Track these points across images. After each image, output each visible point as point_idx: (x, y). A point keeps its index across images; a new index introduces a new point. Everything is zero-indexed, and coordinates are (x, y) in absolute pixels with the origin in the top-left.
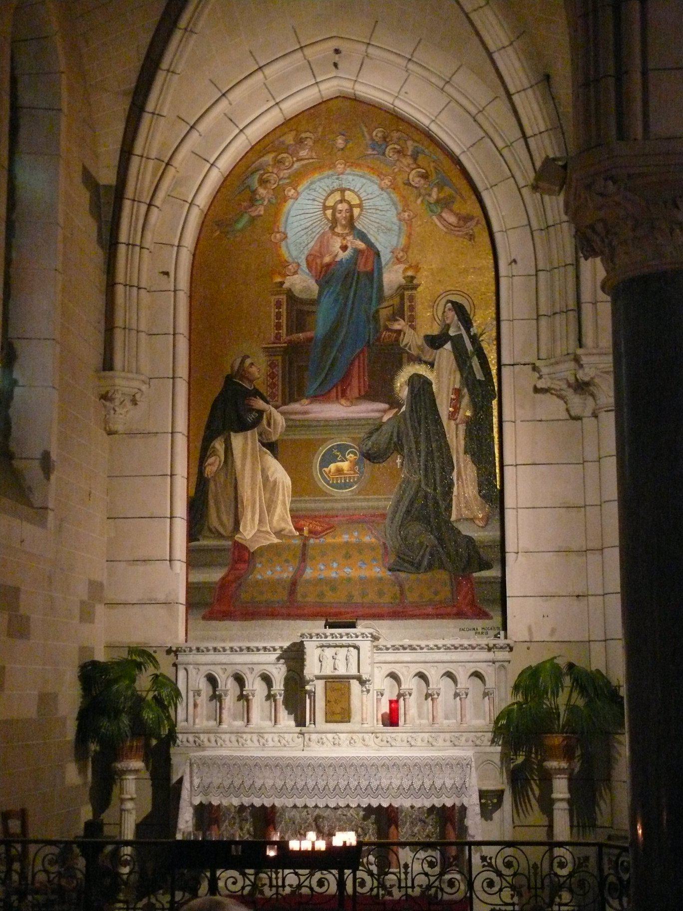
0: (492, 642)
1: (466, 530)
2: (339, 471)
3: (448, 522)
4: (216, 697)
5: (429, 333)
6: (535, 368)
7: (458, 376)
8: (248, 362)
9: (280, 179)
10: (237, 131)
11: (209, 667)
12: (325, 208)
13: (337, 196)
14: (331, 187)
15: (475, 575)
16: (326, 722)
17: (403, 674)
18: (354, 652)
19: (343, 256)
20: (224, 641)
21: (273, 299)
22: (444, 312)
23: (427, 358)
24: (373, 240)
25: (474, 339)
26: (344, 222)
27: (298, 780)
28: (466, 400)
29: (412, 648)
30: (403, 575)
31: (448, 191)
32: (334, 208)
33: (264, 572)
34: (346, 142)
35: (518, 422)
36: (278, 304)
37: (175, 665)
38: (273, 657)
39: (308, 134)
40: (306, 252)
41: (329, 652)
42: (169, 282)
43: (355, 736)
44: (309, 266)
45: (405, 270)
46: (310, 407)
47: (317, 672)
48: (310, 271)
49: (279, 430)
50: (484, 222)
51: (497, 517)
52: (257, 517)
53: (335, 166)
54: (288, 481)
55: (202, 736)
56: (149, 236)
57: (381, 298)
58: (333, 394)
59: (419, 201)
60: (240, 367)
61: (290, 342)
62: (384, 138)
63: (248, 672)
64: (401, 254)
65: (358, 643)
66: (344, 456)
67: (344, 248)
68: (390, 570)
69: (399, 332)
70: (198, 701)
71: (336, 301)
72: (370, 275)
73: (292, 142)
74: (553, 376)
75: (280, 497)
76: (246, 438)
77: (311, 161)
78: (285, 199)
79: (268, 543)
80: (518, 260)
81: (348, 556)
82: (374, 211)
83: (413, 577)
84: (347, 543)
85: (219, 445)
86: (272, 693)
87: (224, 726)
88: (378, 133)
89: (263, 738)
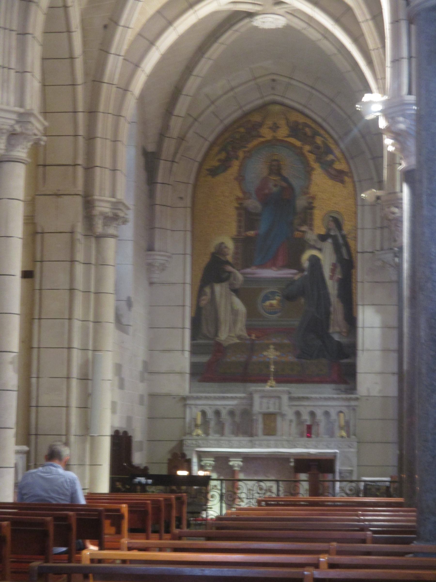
2: (271, 305)
11: (203, 407)
19: (275, 189)
41: (265, 400)
85: (207, 290)
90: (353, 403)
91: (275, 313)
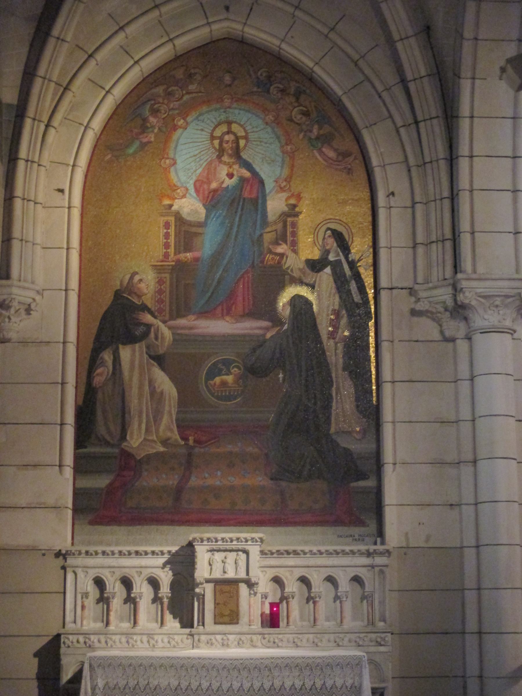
0: (372, 548)
1: (344, 442)
2: (224, 384)
3: (328, 435)
4: (103, 599)
5: (310, 257)
6: (412, 291)
7: (337, 299)
8: (137, 278)
9: (170, 110)
10: (132, 62)
11: (97, 570)
12: (213, 138)
13: (224, 128)
14: (218, 119)
15: (354, 484)
16: (215, 623)
17: (286, 578)
18: (243, 556)
19: (229, 182)
20: (109, 545)
21: (162, 220)
22: (324, 239)
23: (309, 280)
24: (258, 169)
25: (352, 265)
26: (230, 152)
27: (193, 681)
28: (344, 321)
29: (295, 553)
30: (284, 484)
31: (327, 129)
32: (221, 139)
33: (150, 480)
34: (234, 79)
35: (396, 341)
36: (167, 225)
37: (64, 568)
38: (161, 561)
39: (197, 70)
40: (194, 178)
41: (218, 557)
42: (64, 199)
43: (243, 637)
44: (197, 191)
45: (287, 199)
46: (195, 322)
47: (207, 575)
48: (198, 195)
49: (166, 344)
50: (360, 157)
51: (373, 430)
52: (144, 426)
53: (222, 101)
54: (174, 392)
55: (92, 637)
56: (46, 154)
57: (265, 222)
58: (219, 310)
59: (301, 136)
60: (128, 283)
61: (178, 261)
62: (269, 77)
63: (136, 575)
64: (284, 184)
65: (247, 548)
66: (229, 370)
67: (230, 176)
68: (272, 479)
69: (282, 255)
70: (86, 604)
71: (222, 223)
72: (255, 202)
73: (182, 76)
74: (431, 299)
75: (167, 408)
76: (134, 351)
77: (200, 94)
78: (175, 128)
79: (154, 451)
80: (396, 193)
81: (231, 465)
82: (259, 143)
83: (293, 486)
84: (231, 453)
85: (107, 356)
86: (132, 595)
87: (112, 628)
88: (262, 73)
89: (153, 639)
90: (379, 560)
91: (229, 398)
